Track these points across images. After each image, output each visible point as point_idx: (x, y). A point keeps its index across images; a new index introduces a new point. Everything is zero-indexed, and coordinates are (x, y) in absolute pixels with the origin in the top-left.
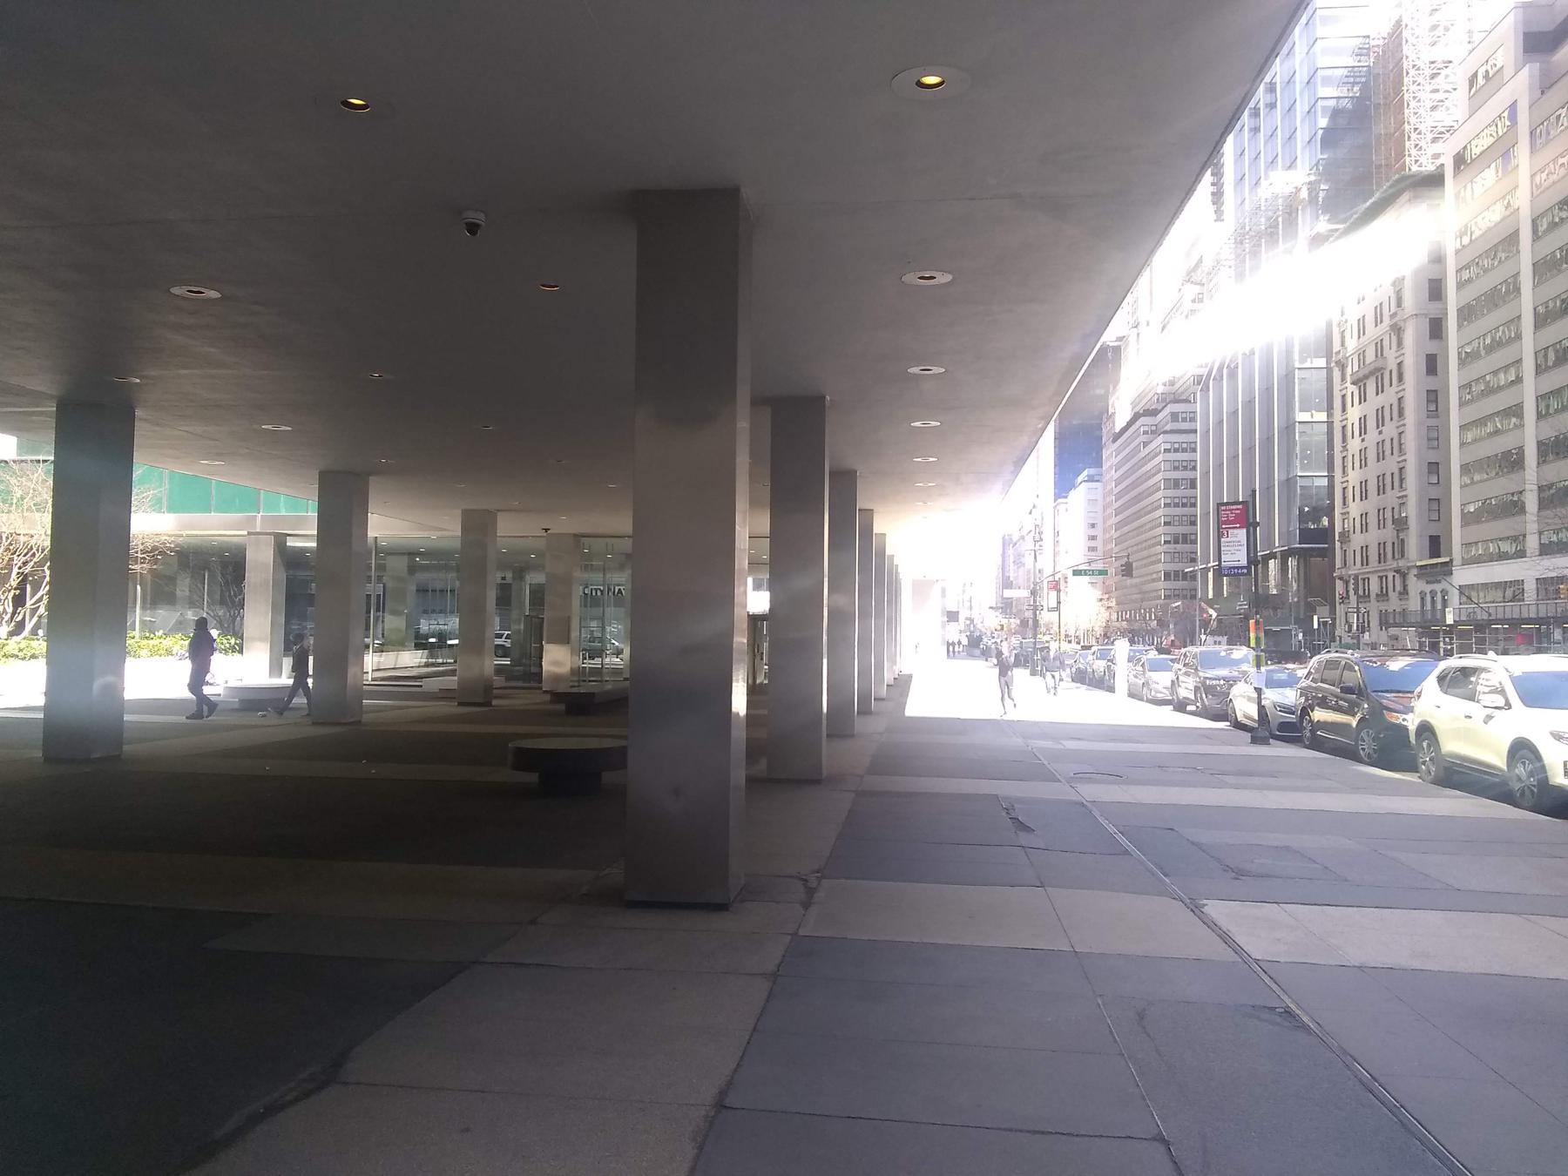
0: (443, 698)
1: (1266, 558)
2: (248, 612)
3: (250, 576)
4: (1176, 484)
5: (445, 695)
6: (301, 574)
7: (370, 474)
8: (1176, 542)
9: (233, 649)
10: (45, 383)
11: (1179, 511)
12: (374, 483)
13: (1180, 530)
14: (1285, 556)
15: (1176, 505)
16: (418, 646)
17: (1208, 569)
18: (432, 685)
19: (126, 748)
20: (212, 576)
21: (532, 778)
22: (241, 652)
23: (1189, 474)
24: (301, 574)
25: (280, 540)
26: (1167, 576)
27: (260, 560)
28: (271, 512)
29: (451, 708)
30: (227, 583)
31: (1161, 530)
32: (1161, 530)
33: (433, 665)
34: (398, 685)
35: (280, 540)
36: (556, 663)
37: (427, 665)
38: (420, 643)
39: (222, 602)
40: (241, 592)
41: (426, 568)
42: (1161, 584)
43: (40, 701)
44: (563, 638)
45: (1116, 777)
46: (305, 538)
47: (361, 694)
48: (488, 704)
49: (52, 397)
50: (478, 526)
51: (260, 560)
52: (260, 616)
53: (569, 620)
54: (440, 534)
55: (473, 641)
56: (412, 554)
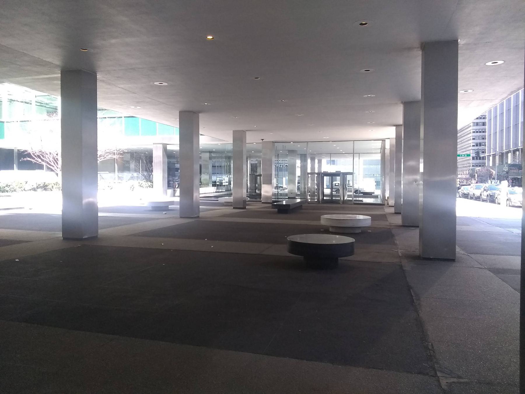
1: (507, 153)
4: (477, 124)
5: (227, 204)
6: (172, 160)
8: (477, 146)
10: (53, 56)
11: (478, 134)
12: (202, 118)
13: (478, 141)
14: (514, 152)
15: (477, 132)
16: (213, 186)
17: (490, 156)
18: (222, 200)
22: (152, 187)
23: (483, 121)
24: (172, 160)
25: (165, 146)
27: (158, 156)
28: (161, 133)
29: (229, 210)
30: (147, 163)
31: (471, 141)
32: (471, 141)
33: (218, 192)
34: (212, 201)
35: (165, 146)
36: (267, 192)
37: (216, 192)
38: (214, 184)
39: (146, 171)
40: (152, 166)
41: (215, 158)
43: (61, 213)
44: (269, 182)
46: (175, 146)
47: (198, 204)
48: (244, 208)
49: (57, 66)
50: (239, 137)
51: (158, 156)
53: (271, 174)
56: (210, 152)
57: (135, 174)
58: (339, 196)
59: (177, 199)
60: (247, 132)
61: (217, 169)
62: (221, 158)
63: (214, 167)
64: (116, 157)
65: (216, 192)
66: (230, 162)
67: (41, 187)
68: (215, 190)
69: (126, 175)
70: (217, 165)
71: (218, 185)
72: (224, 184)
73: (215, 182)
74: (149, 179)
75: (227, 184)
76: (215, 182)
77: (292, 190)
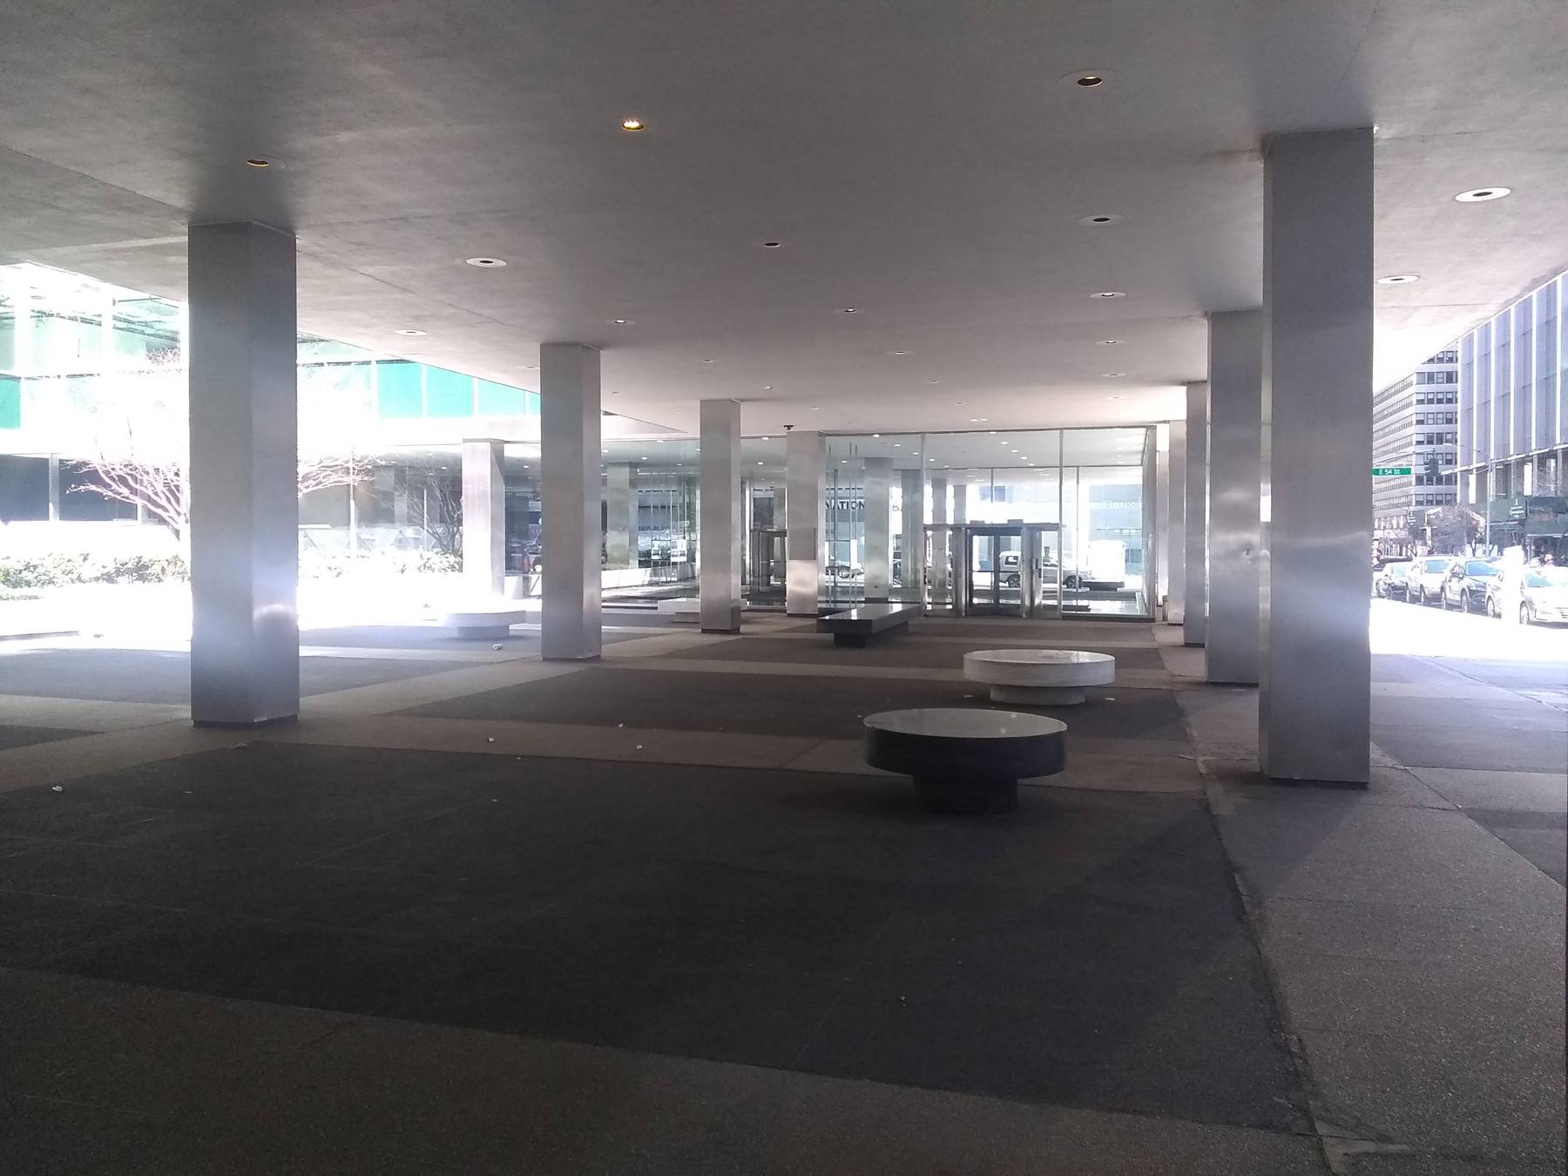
0: (680, 623)
1: (1521, 463)
2: (466, 528)
3: (467, 488)
4: (1431, 378)
5: (683, 620)
6: (522, 490)
7: (601, 346)
8: (1430, 442)
9: (452, 568)
10: (166, 183)
11: (1434, 408)
14: (1542, 460)
15: (1431, 401)
16: (642, 564)
19: (304, 702)
20: (429, 491)
21: (904, 779)
22: (461, 570)
23: (1447, 367)
24: (522, 490)
25: (497, 447)
26: (1419, 480)
27: (478, 477)
28: (484, 408)
29: (692, 637)
32: (1413, 429)
33: (657, 584)
34: (640, 610)
35: (497, 447)
36: (801, 582)
37: (651, 584)
38: (645, 561)
39: (442, 521)
40: (459, 507)
41: (646, 481)
42: (1413, 489)
44: (810, 554)
45: (942, 635)
46: (527, 445)
48: (736, 631)
49: (179, 211)
50: (719, 421)
51: (478, 477)
52: (480, 531)
54: (665, 436)
55: (717, 557)
56: (634, 465)
57: (410, 532)
58: (1017, 595)
59: (535, 606)
60: (745, 409)
61: (653, 516)
62: (667, 481)
63: (643, 508)
64: (352, 479)
65: (651, 584)
66: (691, 493)
67: (129, 572)
68: (647, 579)
69: (383, 534)
70: (652, 501)
71: (656, 563)
72: (673, 559)
73: (648, 554)
74: (450, 544)
75: (684, 559)
76: (648, 554)
77: (876, 577)
